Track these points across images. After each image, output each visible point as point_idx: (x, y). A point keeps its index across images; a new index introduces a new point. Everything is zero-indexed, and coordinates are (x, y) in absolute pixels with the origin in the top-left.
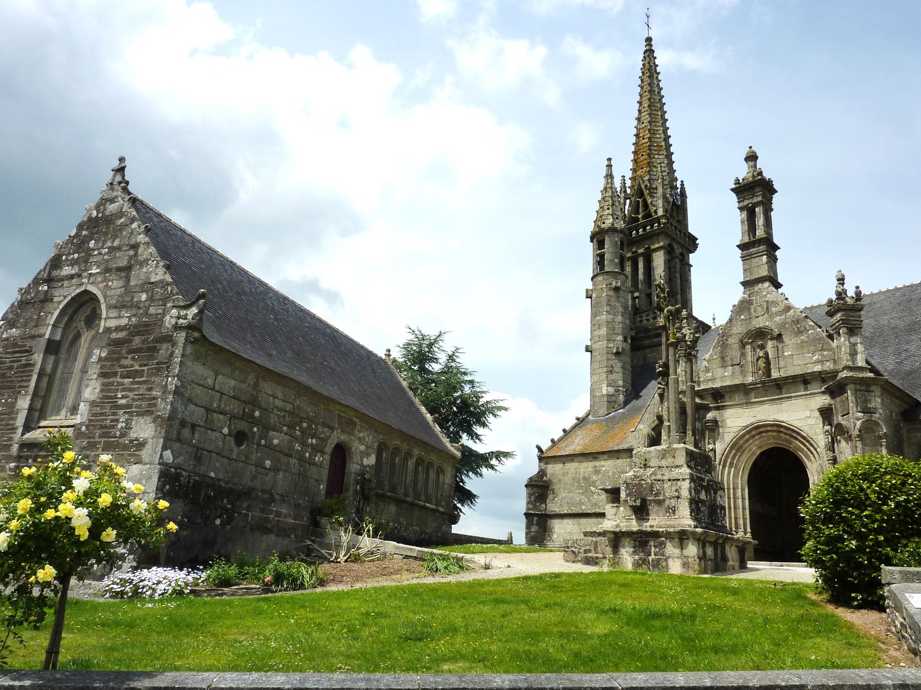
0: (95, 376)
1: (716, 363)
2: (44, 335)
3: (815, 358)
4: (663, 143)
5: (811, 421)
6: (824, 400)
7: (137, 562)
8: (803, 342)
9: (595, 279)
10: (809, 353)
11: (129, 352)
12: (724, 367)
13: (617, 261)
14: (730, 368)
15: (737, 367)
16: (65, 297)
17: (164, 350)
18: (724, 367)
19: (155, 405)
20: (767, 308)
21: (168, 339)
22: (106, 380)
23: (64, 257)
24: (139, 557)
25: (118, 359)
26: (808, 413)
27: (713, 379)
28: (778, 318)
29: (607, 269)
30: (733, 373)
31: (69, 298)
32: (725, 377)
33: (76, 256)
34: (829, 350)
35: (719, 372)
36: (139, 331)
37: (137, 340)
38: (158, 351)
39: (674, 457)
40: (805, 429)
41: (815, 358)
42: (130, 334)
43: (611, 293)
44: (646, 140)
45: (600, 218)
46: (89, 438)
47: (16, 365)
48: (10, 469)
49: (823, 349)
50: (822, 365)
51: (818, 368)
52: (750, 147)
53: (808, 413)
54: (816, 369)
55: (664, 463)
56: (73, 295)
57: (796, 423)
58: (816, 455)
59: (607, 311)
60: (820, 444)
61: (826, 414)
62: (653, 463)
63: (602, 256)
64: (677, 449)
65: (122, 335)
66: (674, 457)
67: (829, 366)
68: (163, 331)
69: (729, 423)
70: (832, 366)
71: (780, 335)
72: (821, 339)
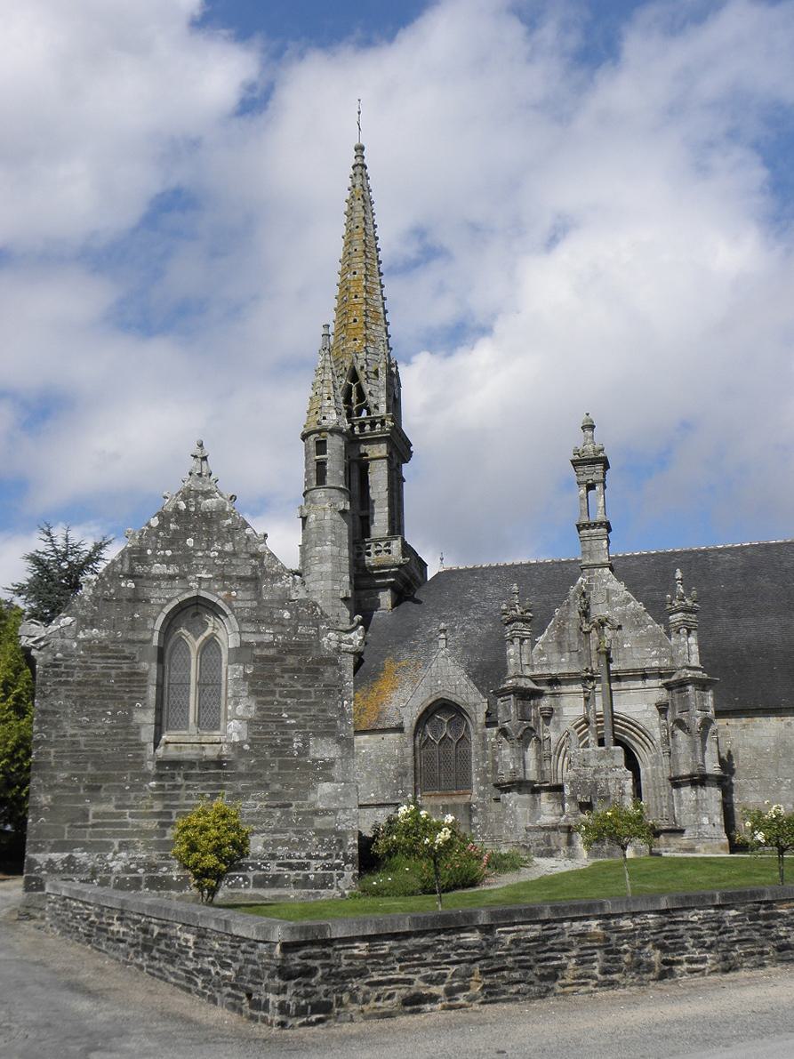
0: (246, 694)
1: (553, 647)
2: (150, 641)
3: (653, 653)
4: (381, 309)
5: (649, 715)
6: (663, 695)
7: (360, 870)
8: (642, 636)
9: (308, 496)
10: (647, 647)
11: (284, 671)
12: (561, 653)
13: (342, 473)
14: (567, 654)
15: (575, 655)
16: (169, 600)
17: (328, 673)
18: (561, 653)
19: (335, 726)
20: (608, 596)
21: (332, 662)
22: (261, 699)
23: (149, 552)
24: (360, 865)
25: (272, 678)
26: (645, 707)
27: (548, 665)
28: (618, 609)
29: (329, 482)
30: (571, 660)
31: (176, 602)
32: (562, 663)
33: (169, 553)
34: (667, 647)
35: (555, 658)
36: (290, 651)
37: (291, 660)
38: (322, 673)
39: (613, 758)
40: (643, 722)
41: (653, 653)
42: (280, 652)
43: (337, 516)
44: (361, 300)
45: (315, 410)
46: (257, 756)
47: (113, 672)
48: (151, 788)
49: (661, 646)
50: (660, 660)
51: (655, 663)
52: (588, 414)
53: (645, 707)
54: (653, 665)
55: (603, 763)
56: (181, 599)
57: (635, 716)
58: (650, 744)
59: (332, 541)
60: (656, 737)
61: (662, 709)
62: (593, 762)
63: (321, 465)
64: (615, 751)
65: (271, 652)
66: (613, 758)
67: (666, 662)
68: (323, 653)
69: (566, 711)
70: (668, 663)
71: (620, 627)
72: (659, 635)
